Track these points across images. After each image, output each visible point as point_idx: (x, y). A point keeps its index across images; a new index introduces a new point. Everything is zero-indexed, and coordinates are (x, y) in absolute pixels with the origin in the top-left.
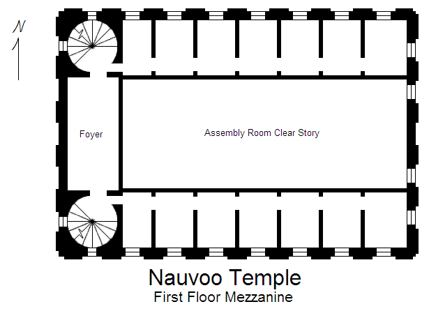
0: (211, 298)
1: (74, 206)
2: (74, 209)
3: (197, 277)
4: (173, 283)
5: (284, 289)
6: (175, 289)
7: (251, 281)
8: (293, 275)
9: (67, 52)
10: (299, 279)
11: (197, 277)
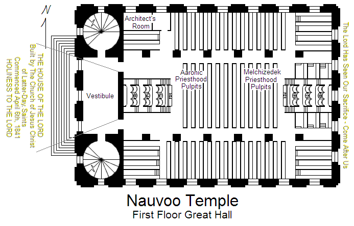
0: (175, 216)
1: (88, 149)
2: (88, 150)
3: (162, 200)
4: (145, 205)
5: (225, 209)
6: (147, 209)
7: (202, 203)
8: (232, 199)
9: (83, 36)
10: (237, 201)
11: (162, 200)
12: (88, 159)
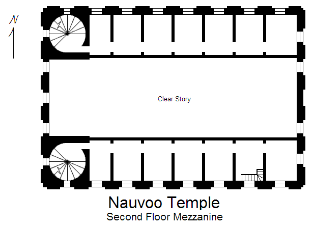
0: (163, 218)
1: (54, 151)
2: (54, 152)
3: (144, 202)
4: (126, 207)
7: (183, 205)
8: (214, 201)
9: (49, 38)
10: (219, 203)
11: (144, 202)
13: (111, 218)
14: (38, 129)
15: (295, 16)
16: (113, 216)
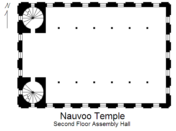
0: (87, 124)
1: (25, 86)
2: (25, 87)
3: (81, 116)
4: (71, 118)
6: (71, 121)
7: (104, 117)
8: (121, 115)
9: (22, 21)
10: (124, 116)
11: (81, 116)
12: (25, 92)
13: (56, 125)
14: (16, 73)
15: (165, 8)
16: (57, 123)
